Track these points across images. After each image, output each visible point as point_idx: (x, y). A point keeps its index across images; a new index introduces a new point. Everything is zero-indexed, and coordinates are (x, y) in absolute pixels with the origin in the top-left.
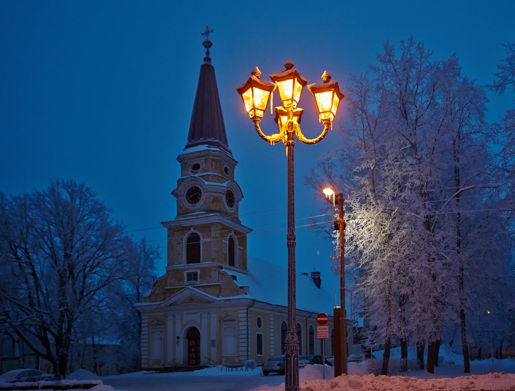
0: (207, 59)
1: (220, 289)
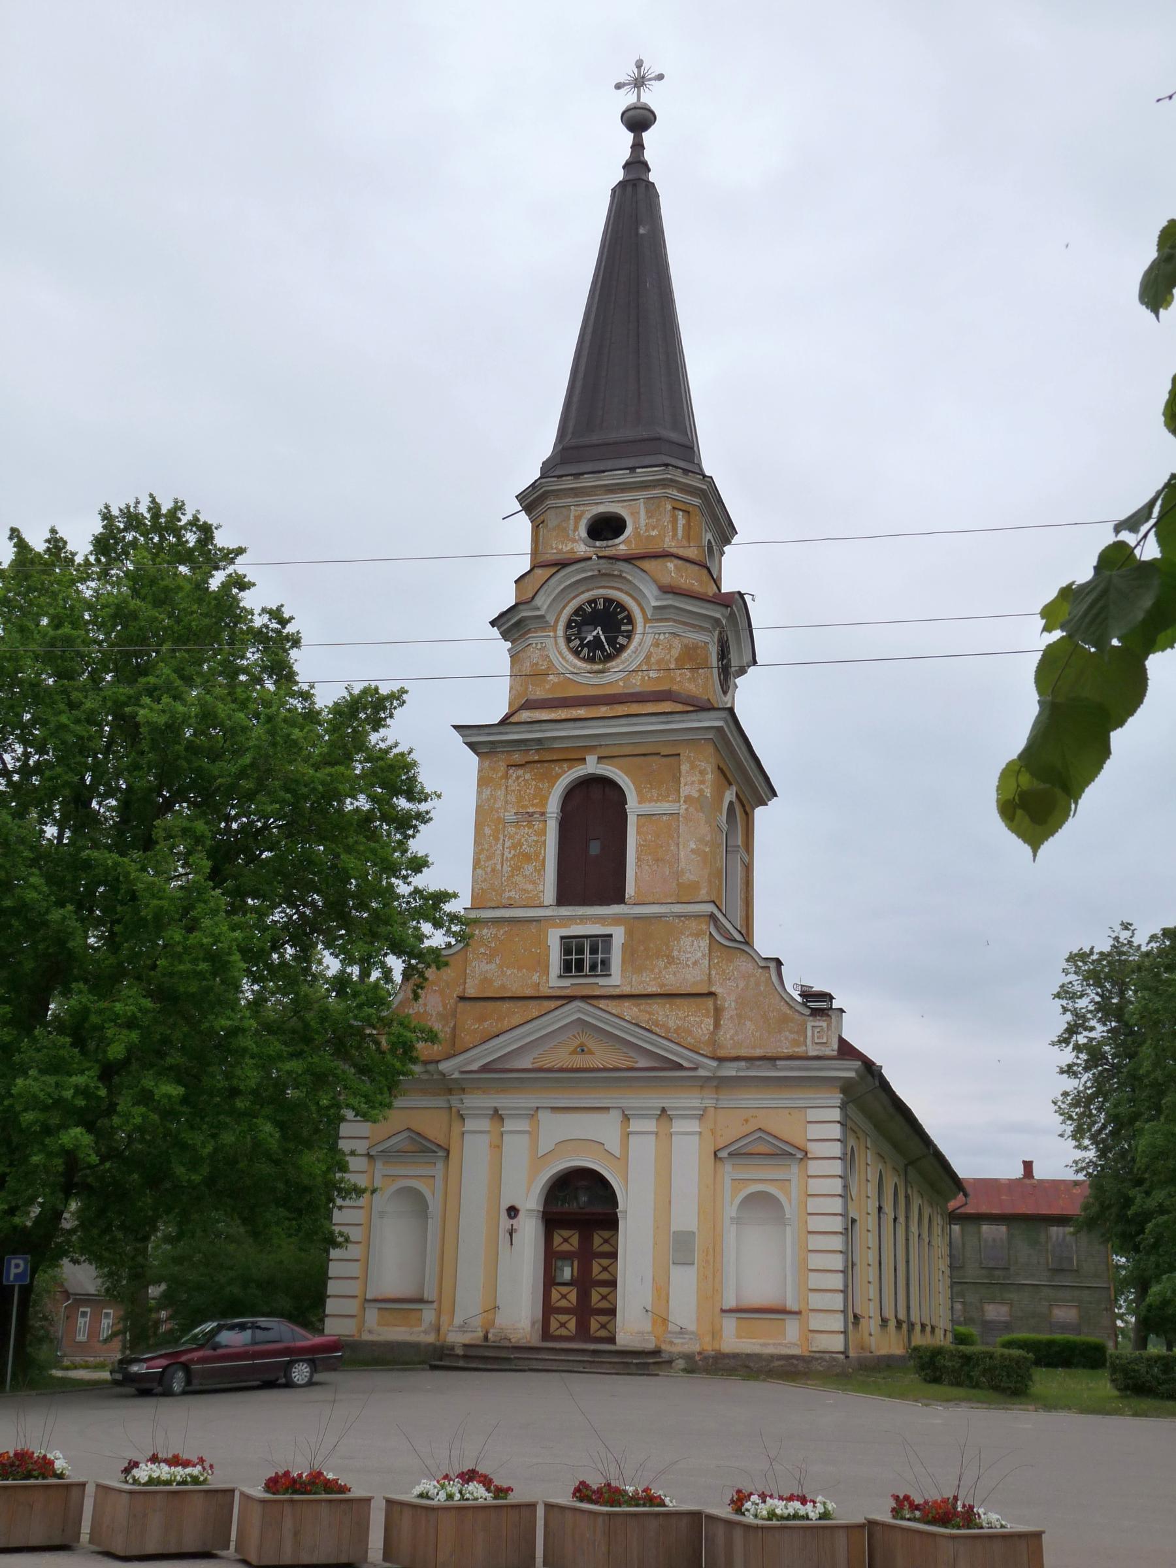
0: (637, 165)
1: (718, 1012)
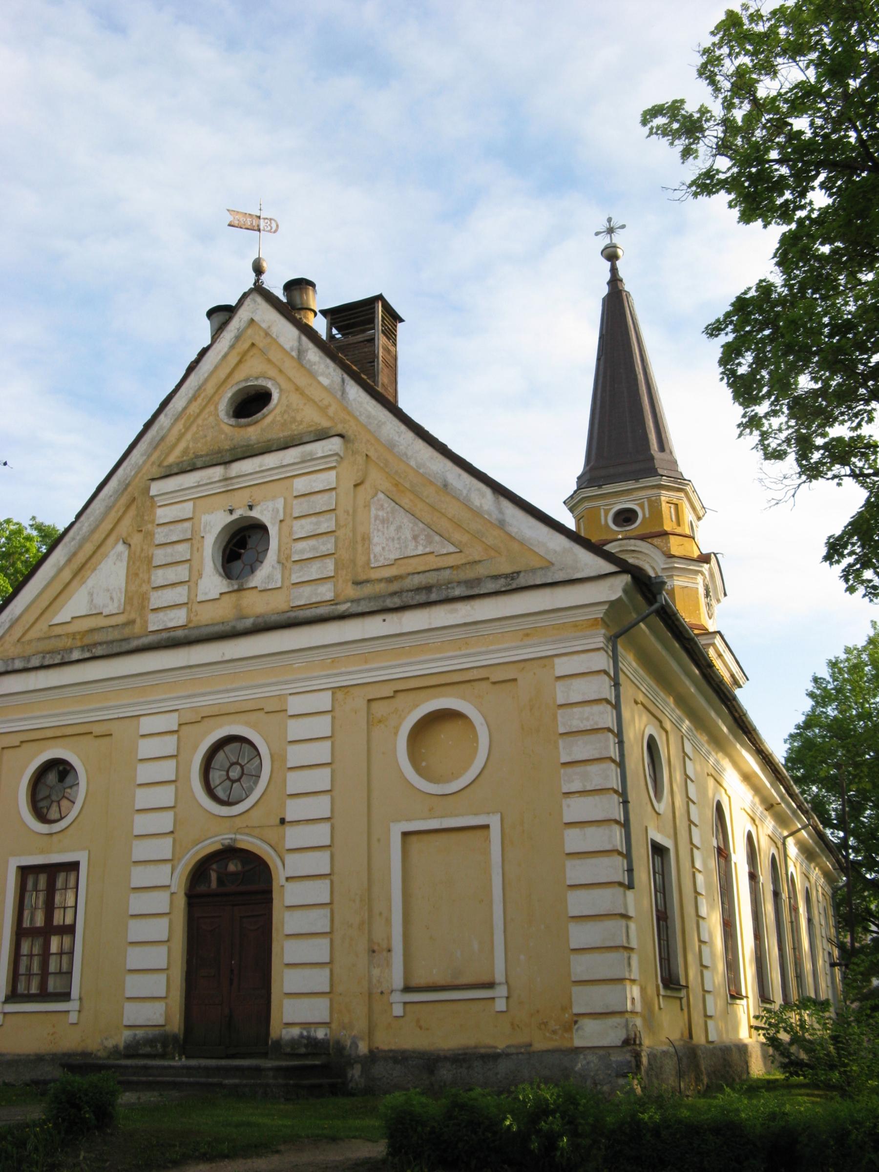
0: (615, 281)
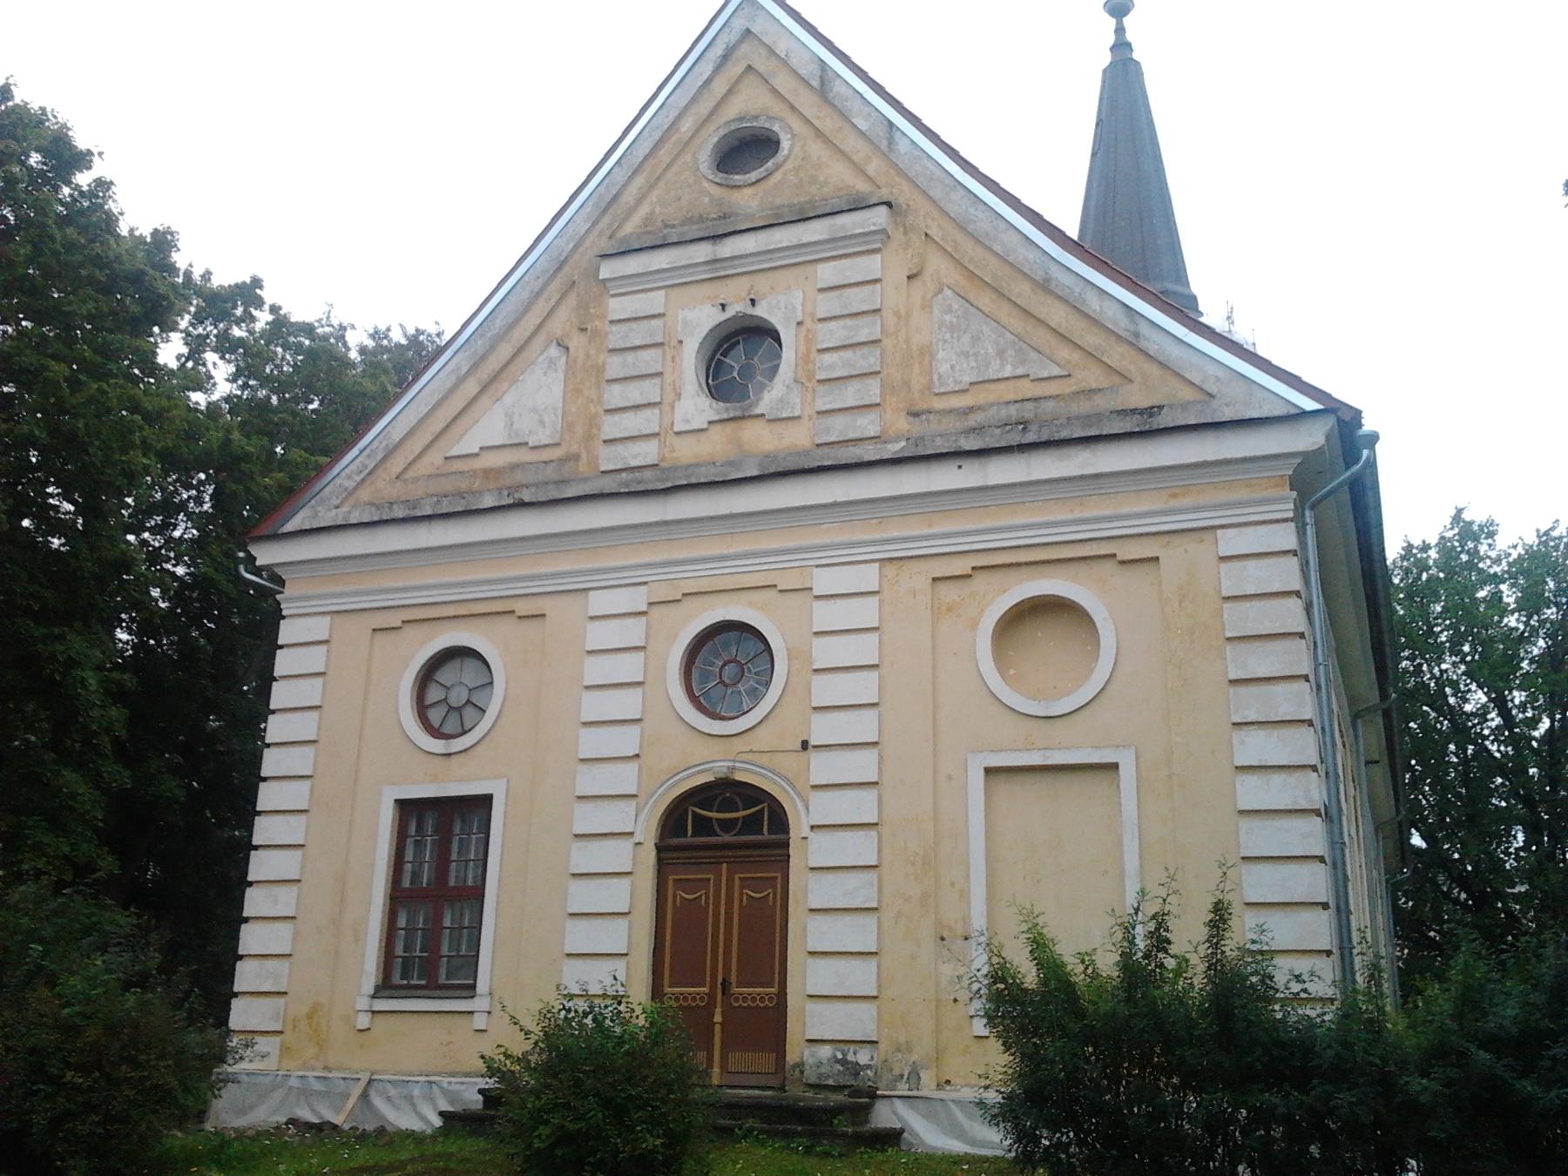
0: (1121, 46)
